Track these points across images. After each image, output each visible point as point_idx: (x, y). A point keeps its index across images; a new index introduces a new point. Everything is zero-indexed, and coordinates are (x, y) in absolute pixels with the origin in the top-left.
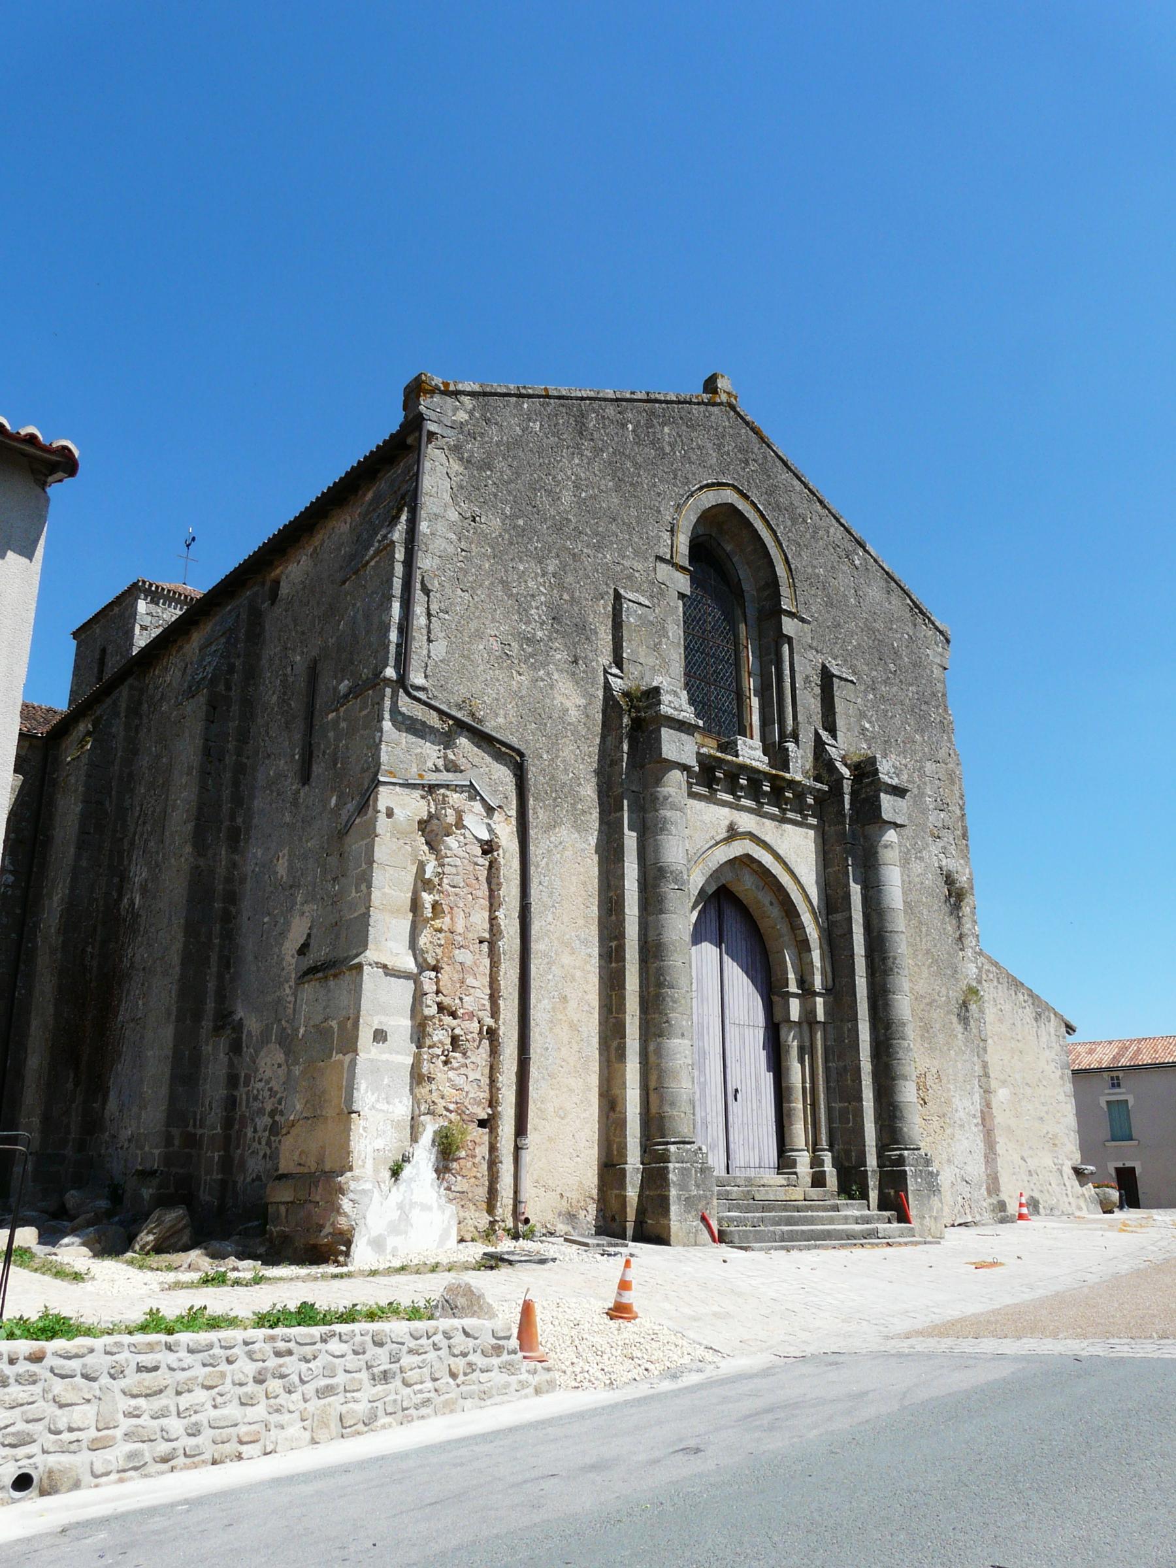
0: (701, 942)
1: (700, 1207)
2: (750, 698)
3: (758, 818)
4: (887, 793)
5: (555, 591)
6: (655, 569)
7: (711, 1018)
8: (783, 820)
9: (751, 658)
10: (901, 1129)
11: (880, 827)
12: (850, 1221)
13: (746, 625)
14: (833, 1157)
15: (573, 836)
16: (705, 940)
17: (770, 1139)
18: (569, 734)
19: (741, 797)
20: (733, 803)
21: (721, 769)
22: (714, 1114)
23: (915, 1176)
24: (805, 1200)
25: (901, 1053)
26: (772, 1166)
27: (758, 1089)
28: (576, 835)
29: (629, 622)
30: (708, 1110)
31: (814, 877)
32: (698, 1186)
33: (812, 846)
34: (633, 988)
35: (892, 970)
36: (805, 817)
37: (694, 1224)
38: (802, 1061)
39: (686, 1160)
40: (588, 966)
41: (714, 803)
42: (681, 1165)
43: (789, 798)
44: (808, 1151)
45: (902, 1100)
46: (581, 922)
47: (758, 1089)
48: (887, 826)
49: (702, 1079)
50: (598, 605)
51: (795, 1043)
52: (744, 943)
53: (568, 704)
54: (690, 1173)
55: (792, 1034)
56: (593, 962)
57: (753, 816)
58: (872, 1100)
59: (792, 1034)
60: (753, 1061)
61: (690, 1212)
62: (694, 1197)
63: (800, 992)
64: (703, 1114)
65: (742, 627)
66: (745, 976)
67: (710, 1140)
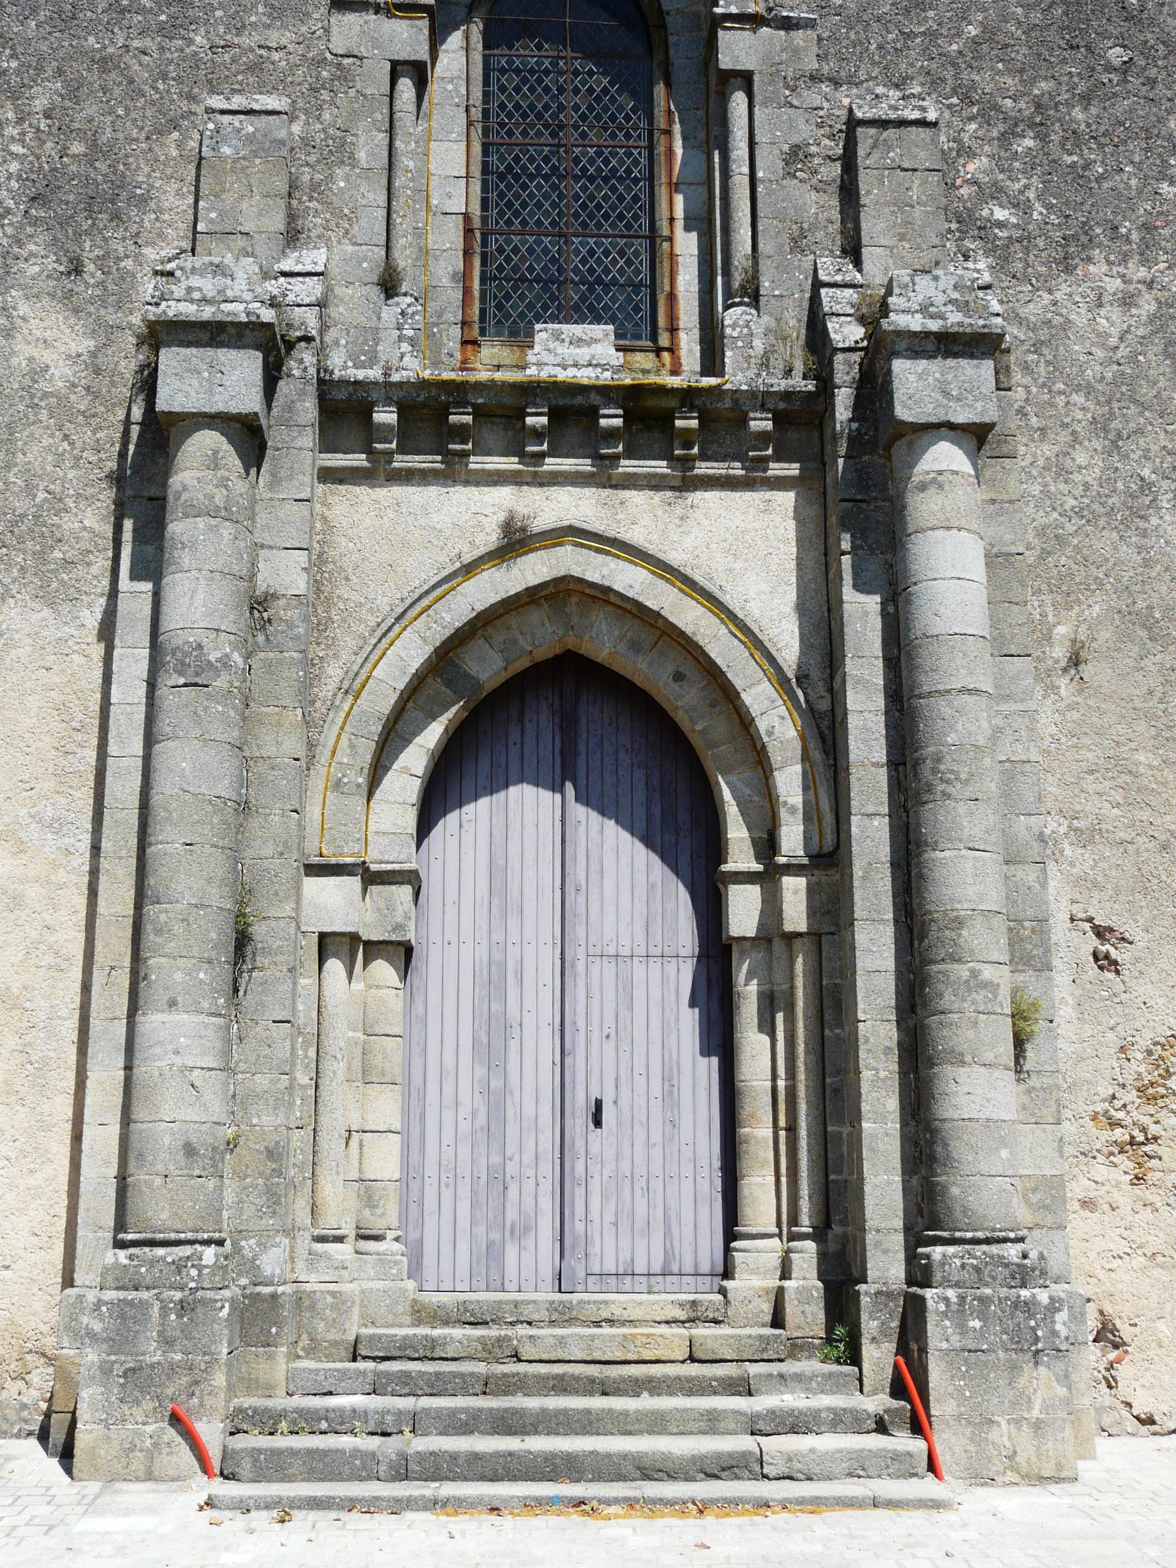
0: (507, 786)
1: (169, 1391)
2: (670, 239)
3: (607, 492)
4: (915, 354)
5: (49, 145)
6: (327, 31)
7: (529, 951)
8: (688, 484)
9: (679, 151)
10: (945, 1188)
11: (911, 443)
12: (296, 1466)
13: (668, 85)
14: (823, 1257)
15: (35, 617)
16: (521, 780)
17: (704, 1212)
18: (44, 415)
19: (542, 455)
20: (519, 472)
21: (465, 404)
22: (528, 1157)
23: (959, 1312)
24: (692, 1359)
25: (948, 996)
26: (705, 1267)
27: (670, 1095)
28: (46, 612)
29: (222, 159)
30: (511, 1149)
31: (792, 595)
32: (167, 1342)
33: (789, 529)
34: (118, 909)
35: (930, 788)
36: (686, 463)
37: (150, 1429)
38: (767, 1026)
39: (148, 1280)
40: (62, 872)
41: (467, 483)
42: (121, 1294)
43: (687, 430)
44: (780, 1236)
45: (946, 1115)
46: (47, 785)
47: (670, 1095)
48: (926, 437)
49: (497, 1084)
50: (163, 144)
51: (753, 987)
52: (639, 775)
53: (47, 356)
54: (147, 1316)
55: (745, 967)
56: (75, 863)
57: (589, 492)
58: (896, 1116)
59: (745, 967)
60: (655, 1033)
61: (137, 1402)
62: (152, 1366)
63: (760, 868)
64: (496, 1159)
65: (660, 90)
66: (640, 847)
67: (511, 1215)
